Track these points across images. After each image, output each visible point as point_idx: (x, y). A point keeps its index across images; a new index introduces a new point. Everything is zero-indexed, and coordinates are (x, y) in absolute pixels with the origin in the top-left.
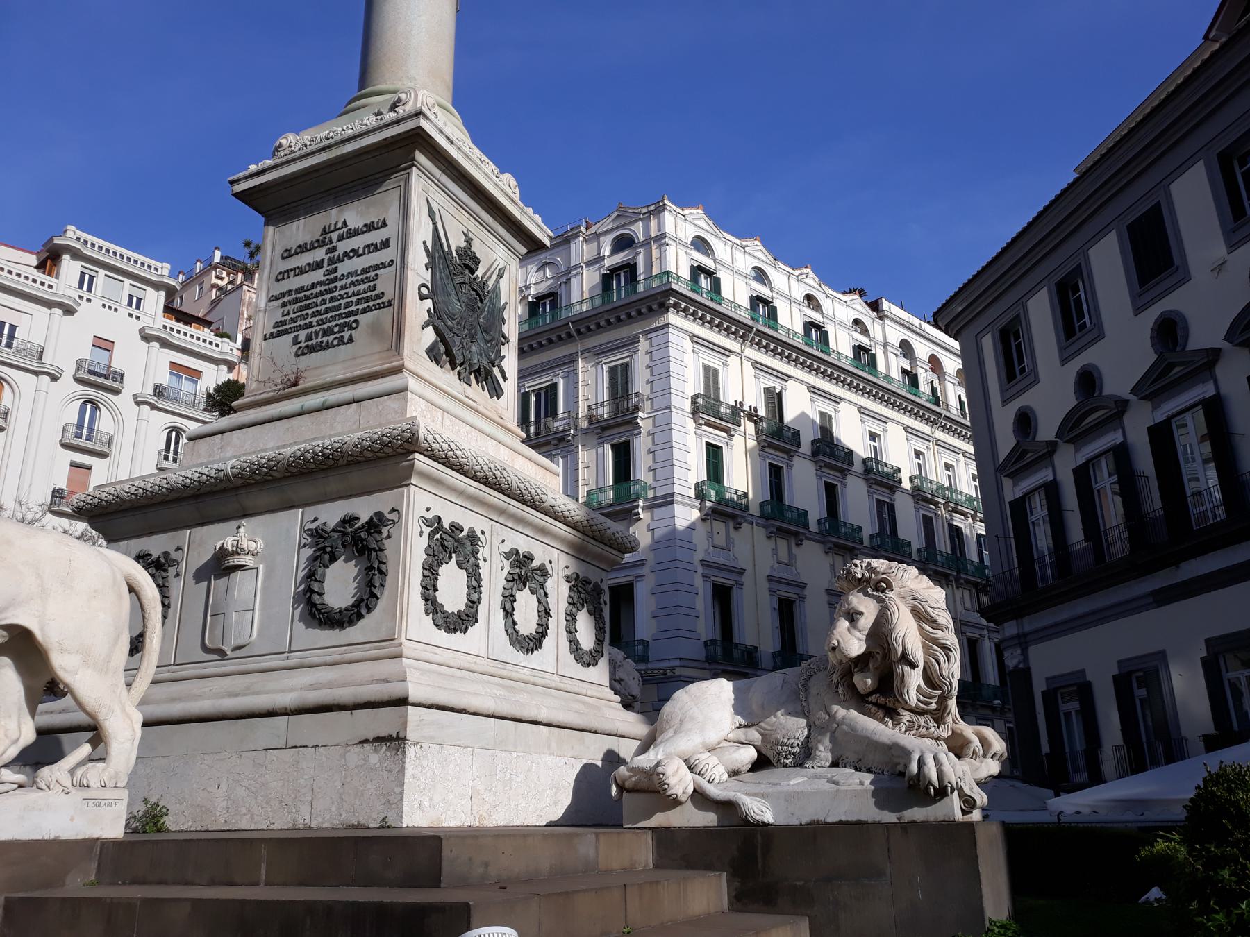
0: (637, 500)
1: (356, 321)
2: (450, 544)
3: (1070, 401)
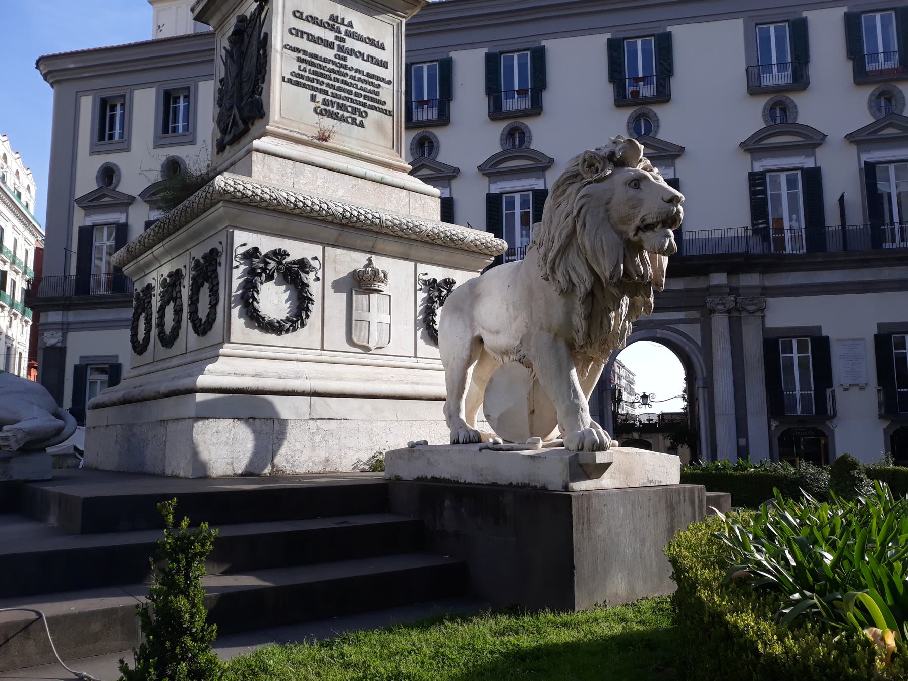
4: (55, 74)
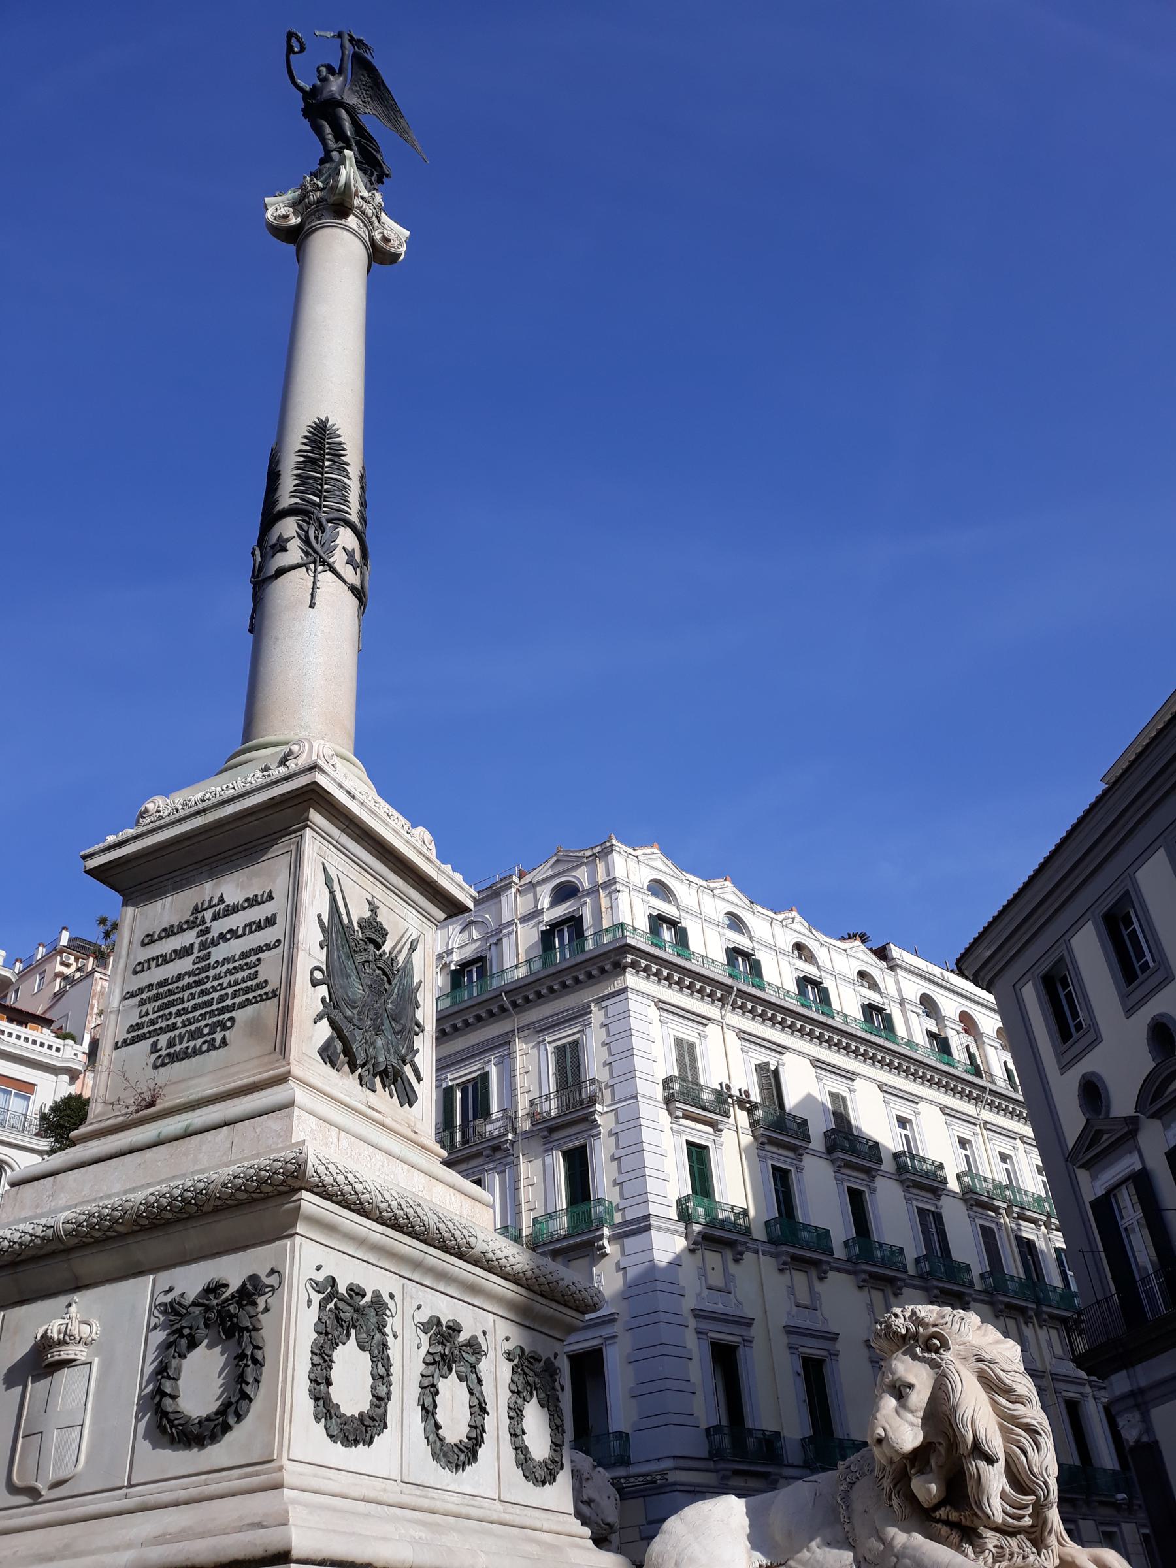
0: (600, 1228)
1: (232, 1019)
2: (350, 1315)
3: (1146, 1064)
4: (982, 974)
